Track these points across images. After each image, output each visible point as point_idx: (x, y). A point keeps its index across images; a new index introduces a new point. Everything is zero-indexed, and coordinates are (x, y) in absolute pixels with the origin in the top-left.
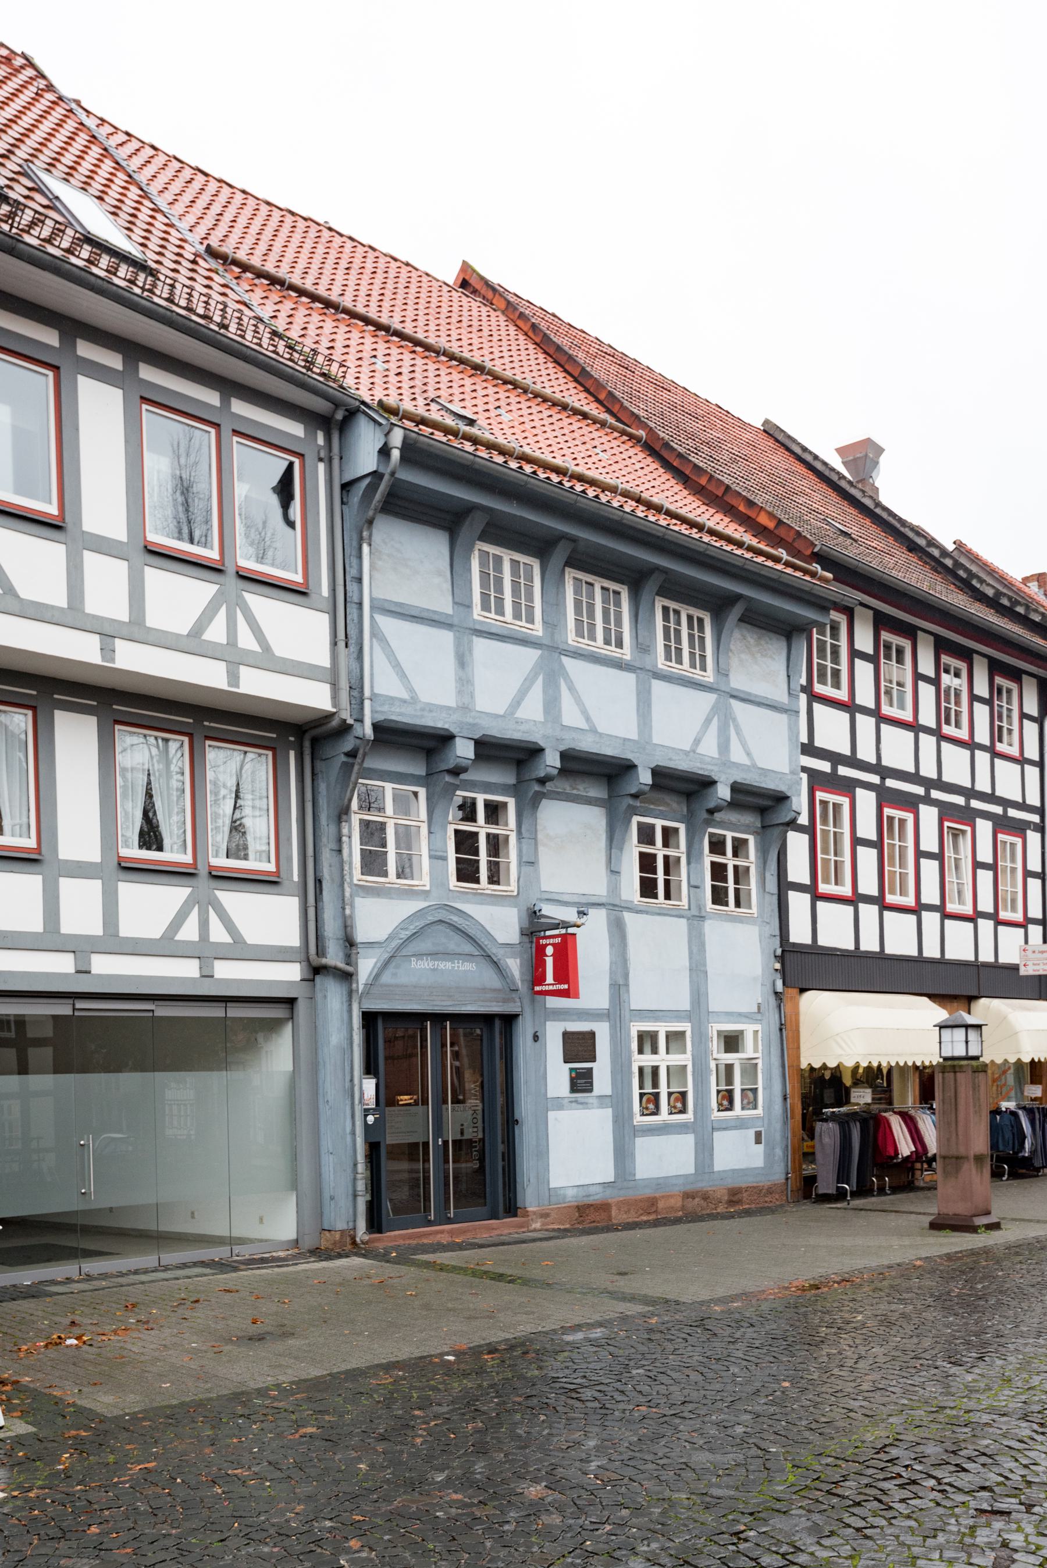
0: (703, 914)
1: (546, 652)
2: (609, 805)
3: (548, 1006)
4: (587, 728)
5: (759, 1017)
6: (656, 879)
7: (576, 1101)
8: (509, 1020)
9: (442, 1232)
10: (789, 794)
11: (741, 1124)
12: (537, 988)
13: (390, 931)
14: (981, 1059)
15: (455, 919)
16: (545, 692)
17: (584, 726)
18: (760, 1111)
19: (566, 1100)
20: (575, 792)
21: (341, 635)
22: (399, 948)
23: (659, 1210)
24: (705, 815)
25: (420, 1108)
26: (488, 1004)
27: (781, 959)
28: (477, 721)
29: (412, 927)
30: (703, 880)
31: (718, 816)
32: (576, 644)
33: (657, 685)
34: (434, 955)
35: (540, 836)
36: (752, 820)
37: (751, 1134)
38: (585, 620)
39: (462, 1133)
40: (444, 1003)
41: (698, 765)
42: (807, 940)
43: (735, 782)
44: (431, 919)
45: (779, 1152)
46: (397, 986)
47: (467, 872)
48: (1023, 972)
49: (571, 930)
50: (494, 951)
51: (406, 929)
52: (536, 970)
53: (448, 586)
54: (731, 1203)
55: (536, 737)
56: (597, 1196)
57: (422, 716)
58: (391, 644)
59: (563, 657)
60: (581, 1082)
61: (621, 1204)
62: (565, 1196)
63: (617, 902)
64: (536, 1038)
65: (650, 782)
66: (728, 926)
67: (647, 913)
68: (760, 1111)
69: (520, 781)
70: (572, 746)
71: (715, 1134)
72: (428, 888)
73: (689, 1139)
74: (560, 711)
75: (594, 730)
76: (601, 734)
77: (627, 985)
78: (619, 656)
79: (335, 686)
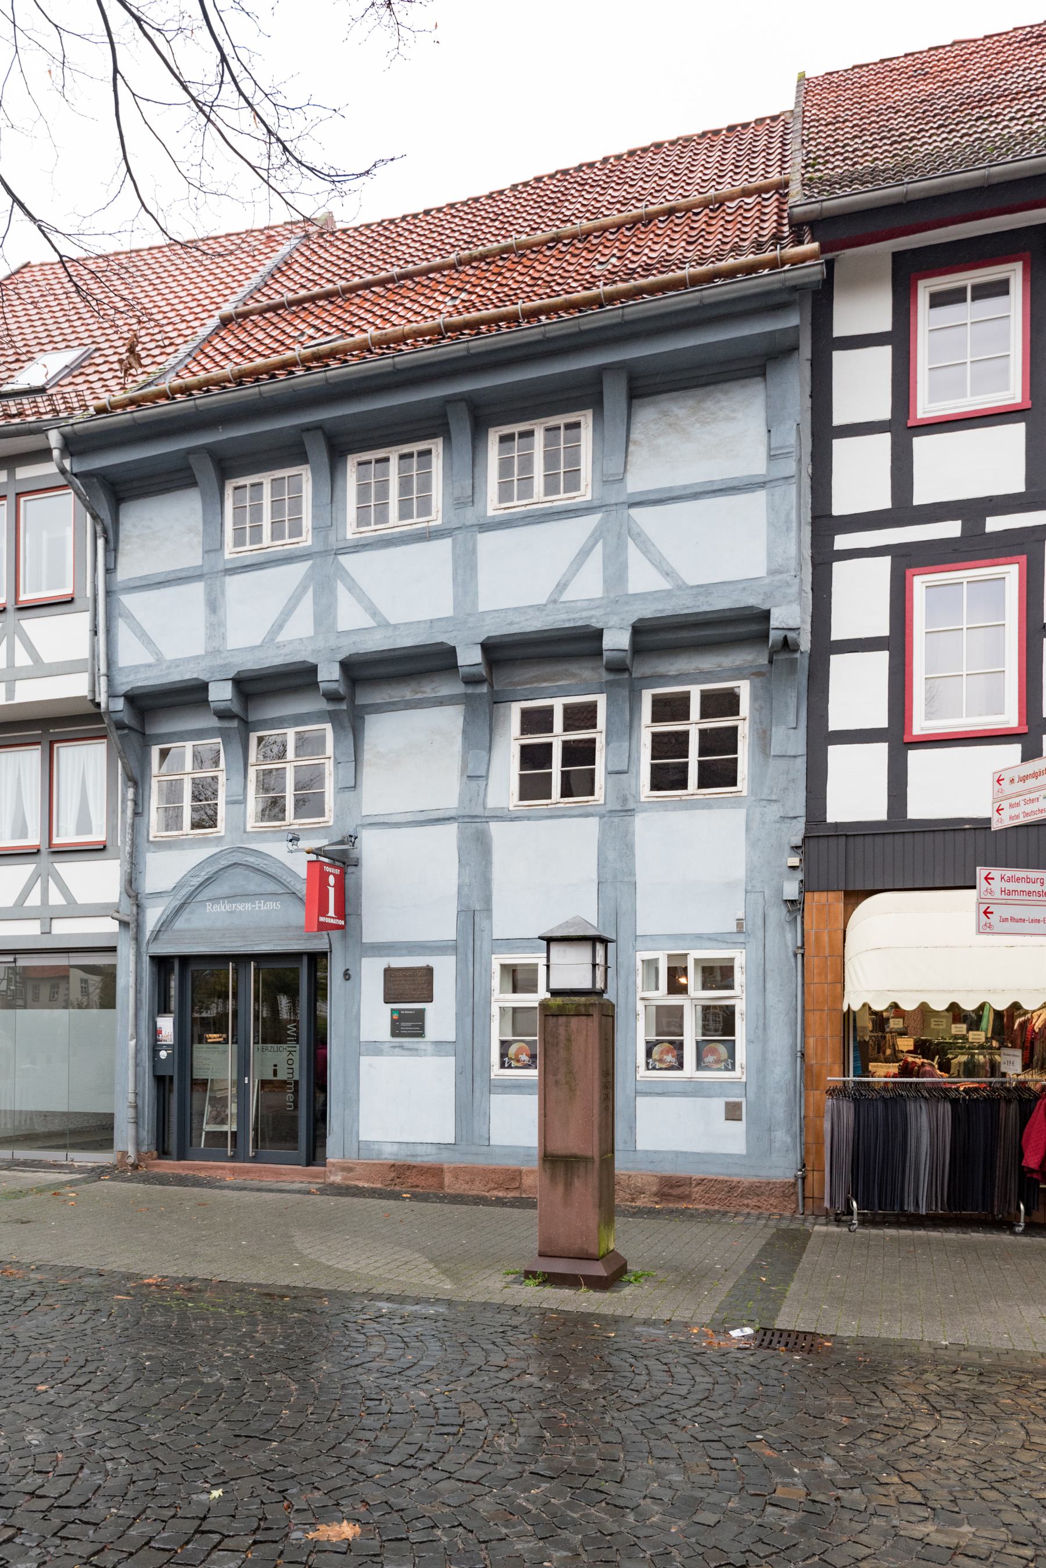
0: (631, 805)
1: (318, 560)
4: (374, 624)
5: (741, 938)
7: (401, 1047)
8: (317, 960)
9: (223, 1168)
11: (695, 1090)
13: (177, 879)
14: (605, 996)
15: (251, 860)
16: (315, 603)
17: (370, 623)
19: (387, 1045)
20: (419, 696)
22: (192, 895)
23: (524, 1187)
28: (227, 661)
29: (203, 873)
32: (358, 536)
34: (231, 898)
35: (367, 755)
37: (718, 1106)
39: (275, 1073)
40: (234, 944)
41: (564, 617)
43: (640, 620)
44: (224, 863)
46: (189, 930)
48: (995, 826)
54: (662, 1195)
55: (304, 655)
56: (428, 1157)
57: (168, 674)
59: (340, 557)
60: (408, 1026)
61: (457, 1172)
62: (380, 1152)
63: (478, 811)
64: (347, 976)
67: (529, 818)
71: (640, 1100)
74: (335, 617)
75: (384, 625)
76: (395, 627)
77: (488, 910)
78: (425, 525)
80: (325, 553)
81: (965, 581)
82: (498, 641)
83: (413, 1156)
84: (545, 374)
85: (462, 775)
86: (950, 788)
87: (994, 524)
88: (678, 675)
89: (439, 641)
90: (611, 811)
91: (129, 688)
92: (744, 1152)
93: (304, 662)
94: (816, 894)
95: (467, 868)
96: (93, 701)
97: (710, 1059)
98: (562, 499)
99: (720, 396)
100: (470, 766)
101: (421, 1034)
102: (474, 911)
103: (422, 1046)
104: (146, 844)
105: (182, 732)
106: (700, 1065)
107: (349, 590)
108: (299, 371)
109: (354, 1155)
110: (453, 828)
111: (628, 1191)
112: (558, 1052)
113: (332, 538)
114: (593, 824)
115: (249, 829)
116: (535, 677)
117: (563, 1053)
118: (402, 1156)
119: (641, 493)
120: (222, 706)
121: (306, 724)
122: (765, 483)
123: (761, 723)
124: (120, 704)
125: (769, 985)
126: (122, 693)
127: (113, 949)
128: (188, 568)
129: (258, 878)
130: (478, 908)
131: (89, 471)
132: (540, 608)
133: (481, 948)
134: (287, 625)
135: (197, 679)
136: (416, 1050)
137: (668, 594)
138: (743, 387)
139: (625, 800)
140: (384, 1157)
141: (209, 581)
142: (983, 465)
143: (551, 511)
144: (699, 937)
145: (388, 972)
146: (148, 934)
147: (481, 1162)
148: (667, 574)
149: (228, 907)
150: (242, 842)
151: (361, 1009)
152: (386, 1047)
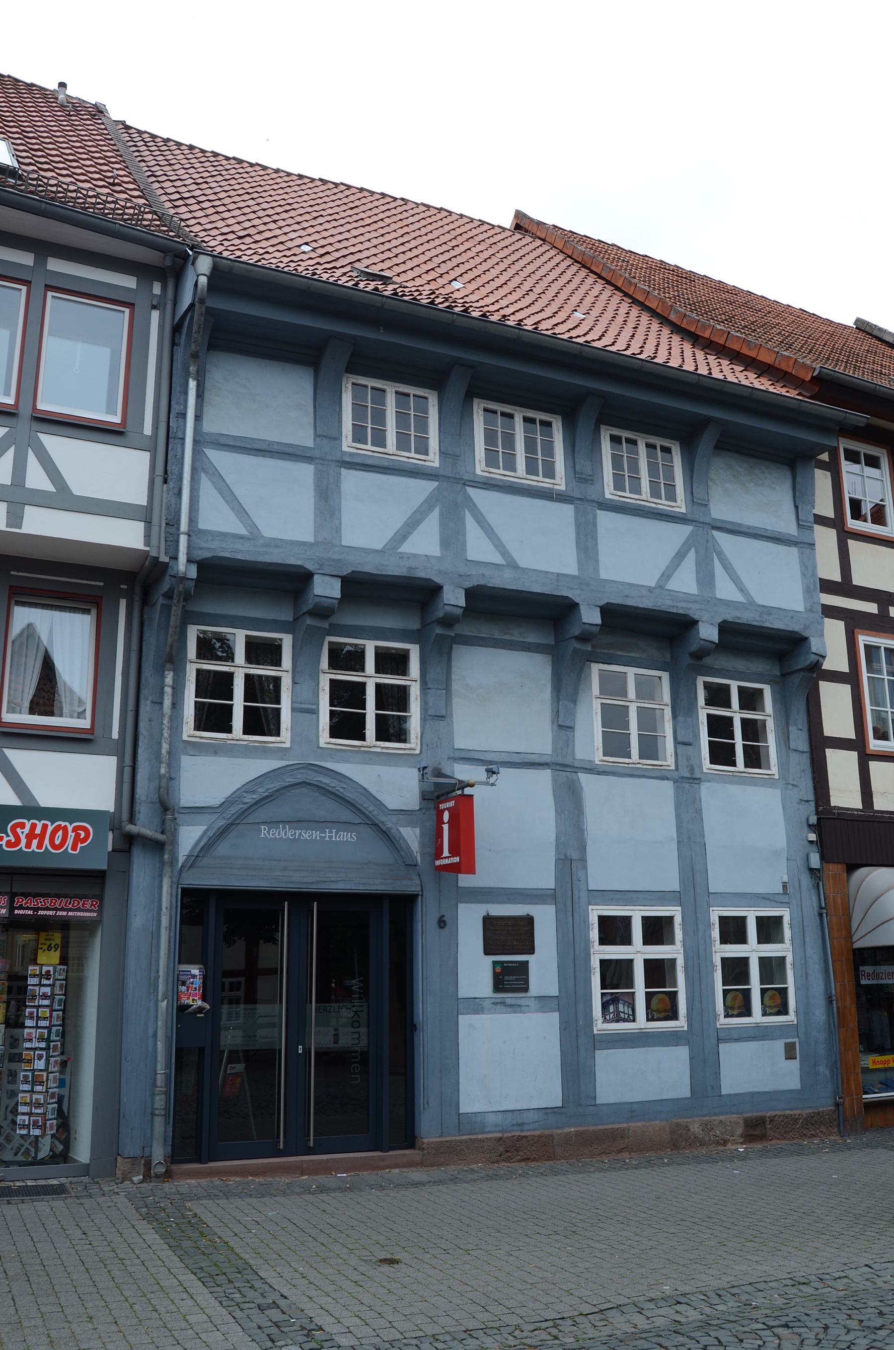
0: (697, 775)
2: (554, 652)
3: (460, 885)
4: (504, 563)
6: (734, 744)
8: (402, 907)
10: (806, 634)
11: (760, 1034)
12: (438, 863)
13: (228, 793)
15: (325, 780)
17: (499, 560)
20: (507, 637)
21: (160, 470)
22: (243, 814)
24: (688, 660)
29: (261, 790)
30: (697, 736)
31: (709, 661)
33: (604, 518)
35: (455, 686)
36: (767, 667)
37: (779, 1046)
38: (501, 450)
40: (304, 880)
41: (670, 603)
42: (856, 803)
43: (725, 622)
45: (823, 1070)
47: (347, 726)
49: (468, 791)
50: (383, 819)
51: (254, 792)
52: (437, 842)
53: (311, 419)
59: (468, 488)
60: (510, 980)
63: (568, 761)
64: (442, 923)
66: (734, 790)
68: (791, 1017)
69: (424, 626)
70: (482, 583)
72: (288, 745)
73: (683, 1052)
76: (524, 570)
77: (583, 860)
78: (551, 486)
79: (148, 523)
81: (883, 646)
85: (553, 723)
90: (683, 777)
93: (429, 580)
94: (831, 865)
100: (561, 715)
102: (571, 859)
103: (523, 1002)
110: (547, 773)
115: (322, 744)
124: (193, 573)
125: (807, 939)
126: (199, 559)
130: (574, 857)
132: (650, 590)
133: (579, 899)
134: (412, 538)
136: (520, 1006)
139: (692, 770)
141: (320, 467)
143: (656, 511)
146: (181, 860)
148: (742, 589)
149: (289, 834)
152: (487, 1004)
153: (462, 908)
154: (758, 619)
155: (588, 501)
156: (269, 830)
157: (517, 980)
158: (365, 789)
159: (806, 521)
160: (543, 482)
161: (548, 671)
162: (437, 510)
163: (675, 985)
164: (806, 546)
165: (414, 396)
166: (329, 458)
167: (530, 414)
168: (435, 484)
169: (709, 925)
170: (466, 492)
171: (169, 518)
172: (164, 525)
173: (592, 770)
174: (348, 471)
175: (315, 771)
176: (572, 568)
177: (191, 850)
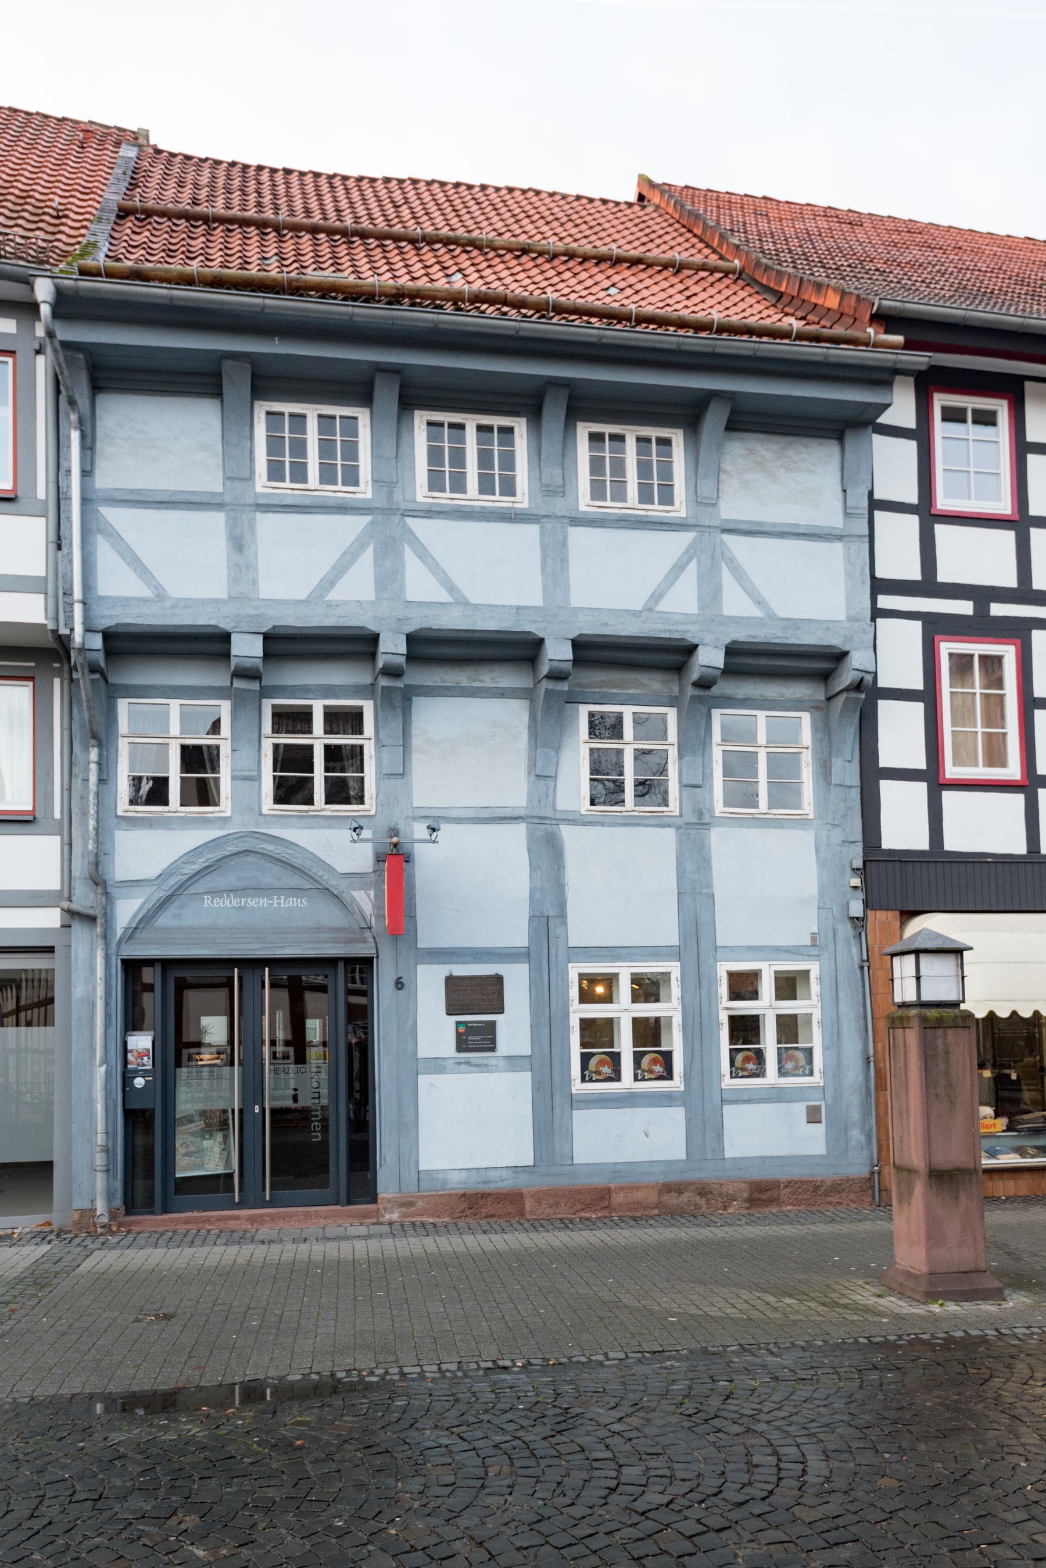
0: (707, 820)
1: (380, 518)
4: (452, 601)
5: (815, 951)
7: (468, 1063)
8: (361, 968)
11: (778, 1096)
13: (165, 864)
14: (963, 1007)
15: (269, 847)
16: (377, 564)
17: (444, 597)
18: (817, 1079)
19: (451, 1062)
20: (476, 684)
22: (183, 886)
25: (226, 1070)
26: (321, 945)
27: (863, 871)
28: (260, 611)
29: (201, 860)
35: (415, 742)
37: (800, 1110)
39: (295, 1099)
41: (660, 626)
42: (921, 842)
43: (734, 642)
44: (231, 849)
46: (180, 929)
47: (291, 790)
51: (193, 863)
55: (366, 621)
56: (507, 1183)
58: (126, 539)
60: (477, 1040)
61: (540, 1196)
62: (445, 1182)
63: (549, 813)
65: (570, 656)
66: (754, 835)
70: (426, 624)
73: (678, 1114)
76: (476, 606)
77: (562, 916)
78: (510, 505)
80: (388, 511)
82: (589, 639)
83: (485, 1183)
84: (663, 384)
85: (529, 773)
86: (984, 825)
87: (998, 610)
88: (745, 700)
89: (527, 629)
90: (688, 824)
91: (113, 623)
92: (824, 1153)
95: (539, 871)
96: (55, 632)
97: (789, 1065)
98: (656, 510)
99: (801, 448)
100: (539, 764)
101: (492, 1047)
102: (548, 916)
103: (493, 1062)
104: (115, 820)
105: (164, 687)
106: (782, 1072)
107: (420, 558)
108: (449, 307)
109: (413, 1188)
110: (521, 829)
111: (720, 1199)
112: (937, 1065)
113: (398, 496)
114: (669, 835)
115: (265, 811)
116: (603, 681)
117: (942, 1066)
118: (475, 1185)
119: (734, 521)
120: (248, 663)
121: (338, 698)
122: (842, 536)
123: (822, 753)
124: (97, 642)
125: (841, 995)
126: (101, 628)
127: (50, 950)
128: (204, 493)
129: (276, 869)
130: (551, 914)
131: (78, 343)
132: (636, 614)
133: (557, 956)
135: (215, 626)
136: (486, 1065)
137: (759, 622)
138: (820, 445)
139: (701, 814)
140: (449, 1186)
141: (232, 514)
142: (977, 558)
143: (645, 519)
144: (777, 949)
145: (450, 980)
147: (563, 1182)
148: (760, 602)
150: (257, 825)
151: (420, 1020)
153: (422, 969)
154: (780, 635)
155: (557, 517)
156: (213, 899)
157: (482, 1040)
158: (312, 854)
159: (857, 508)
160: (503, 502)
161: (525, 717)
162: (371, 547)
163: (811, 1040)
164: (854, 539)
165: (341, 417)
166: (242, 502)
167: (486, 420)
168: (368, 519)
169: (714, 981)
170: (405, 523)
171: (66, 587)
172: (61, 595)
173: (574, 820)
174: (265, 515)
175: (257, 838)
176: (534, 598)
177: (130, 923)
